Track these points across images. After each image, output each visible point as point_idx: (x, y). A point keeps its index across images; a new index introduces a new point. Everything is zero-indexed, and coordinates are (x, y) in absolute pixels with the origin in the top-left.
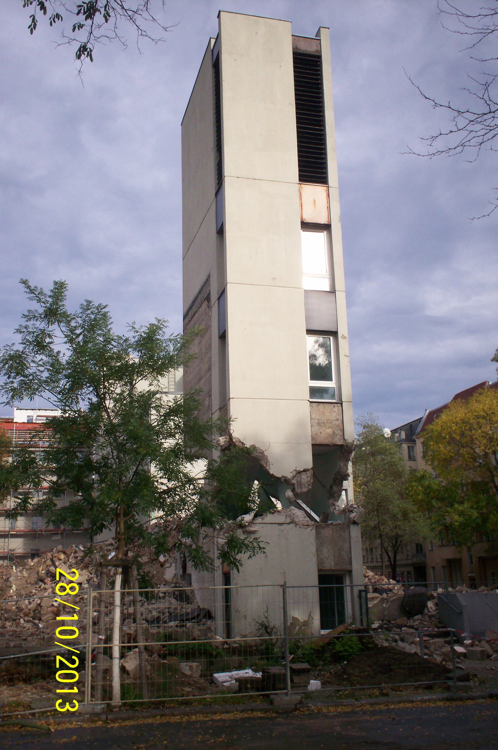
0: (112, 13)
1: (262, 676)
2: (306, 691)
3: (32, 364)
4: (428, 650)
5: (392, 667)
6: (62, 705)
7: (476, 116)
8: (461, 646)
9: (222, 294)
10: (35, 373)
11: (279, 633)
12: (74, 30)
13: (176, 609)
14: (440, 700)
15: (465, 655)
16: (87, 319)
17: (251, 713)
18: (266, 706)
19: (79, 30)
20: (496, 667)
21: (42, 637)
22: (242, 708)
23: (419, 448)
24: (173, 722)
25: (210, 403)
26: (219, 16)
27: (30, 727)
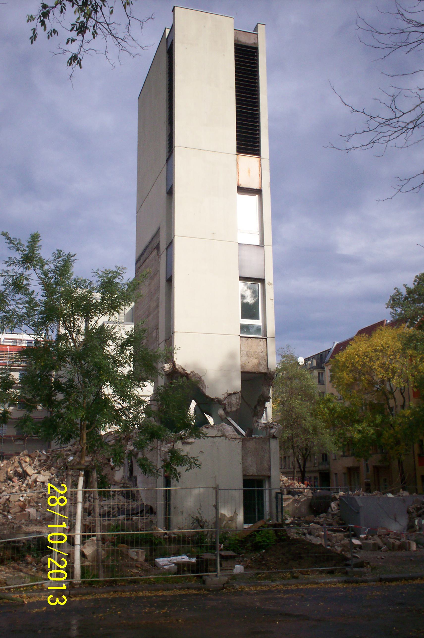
0: (99, 31)
1: (196, 561)
2: (231, 574)
3: (12, 302)
4: (331, 542)
5: (302, 555)
6: (52, 601)
7: (385, 120)
8: (358, 539)
9: (170, 244)
10: (14, 309)
11: (210, 527)
12: (67, 43)
13: (124, 505)
14: (339, 582)
15: (360, 547)
16: (58, 265)
17: (188, 591)
18: (200, 585)
19: (72, 43)
20: (385, 557)
21: (12, 526)
22: (180, 587)
23: (327, 374)
24: (124, 597)
25: (157, 335)
26: (173, 10)
27: (6, 599)
